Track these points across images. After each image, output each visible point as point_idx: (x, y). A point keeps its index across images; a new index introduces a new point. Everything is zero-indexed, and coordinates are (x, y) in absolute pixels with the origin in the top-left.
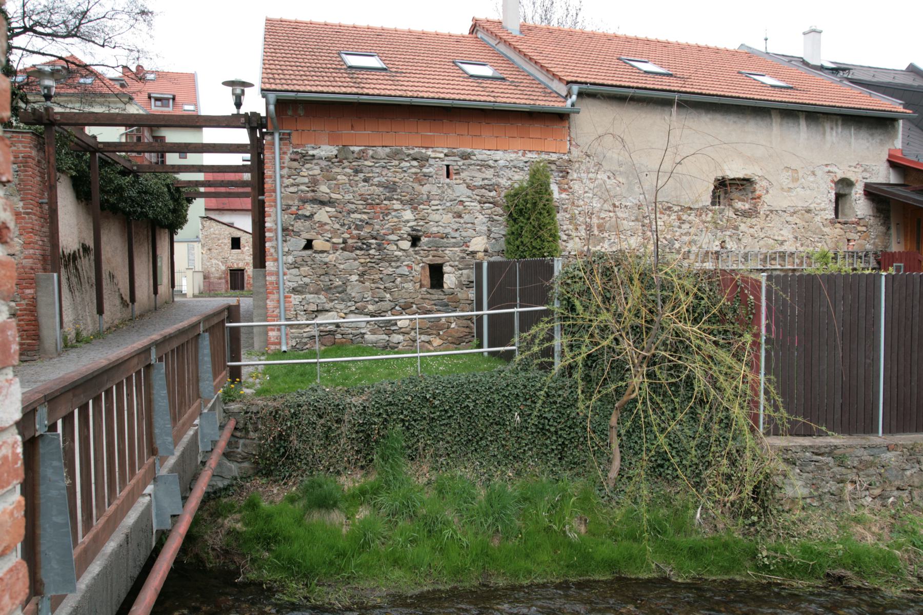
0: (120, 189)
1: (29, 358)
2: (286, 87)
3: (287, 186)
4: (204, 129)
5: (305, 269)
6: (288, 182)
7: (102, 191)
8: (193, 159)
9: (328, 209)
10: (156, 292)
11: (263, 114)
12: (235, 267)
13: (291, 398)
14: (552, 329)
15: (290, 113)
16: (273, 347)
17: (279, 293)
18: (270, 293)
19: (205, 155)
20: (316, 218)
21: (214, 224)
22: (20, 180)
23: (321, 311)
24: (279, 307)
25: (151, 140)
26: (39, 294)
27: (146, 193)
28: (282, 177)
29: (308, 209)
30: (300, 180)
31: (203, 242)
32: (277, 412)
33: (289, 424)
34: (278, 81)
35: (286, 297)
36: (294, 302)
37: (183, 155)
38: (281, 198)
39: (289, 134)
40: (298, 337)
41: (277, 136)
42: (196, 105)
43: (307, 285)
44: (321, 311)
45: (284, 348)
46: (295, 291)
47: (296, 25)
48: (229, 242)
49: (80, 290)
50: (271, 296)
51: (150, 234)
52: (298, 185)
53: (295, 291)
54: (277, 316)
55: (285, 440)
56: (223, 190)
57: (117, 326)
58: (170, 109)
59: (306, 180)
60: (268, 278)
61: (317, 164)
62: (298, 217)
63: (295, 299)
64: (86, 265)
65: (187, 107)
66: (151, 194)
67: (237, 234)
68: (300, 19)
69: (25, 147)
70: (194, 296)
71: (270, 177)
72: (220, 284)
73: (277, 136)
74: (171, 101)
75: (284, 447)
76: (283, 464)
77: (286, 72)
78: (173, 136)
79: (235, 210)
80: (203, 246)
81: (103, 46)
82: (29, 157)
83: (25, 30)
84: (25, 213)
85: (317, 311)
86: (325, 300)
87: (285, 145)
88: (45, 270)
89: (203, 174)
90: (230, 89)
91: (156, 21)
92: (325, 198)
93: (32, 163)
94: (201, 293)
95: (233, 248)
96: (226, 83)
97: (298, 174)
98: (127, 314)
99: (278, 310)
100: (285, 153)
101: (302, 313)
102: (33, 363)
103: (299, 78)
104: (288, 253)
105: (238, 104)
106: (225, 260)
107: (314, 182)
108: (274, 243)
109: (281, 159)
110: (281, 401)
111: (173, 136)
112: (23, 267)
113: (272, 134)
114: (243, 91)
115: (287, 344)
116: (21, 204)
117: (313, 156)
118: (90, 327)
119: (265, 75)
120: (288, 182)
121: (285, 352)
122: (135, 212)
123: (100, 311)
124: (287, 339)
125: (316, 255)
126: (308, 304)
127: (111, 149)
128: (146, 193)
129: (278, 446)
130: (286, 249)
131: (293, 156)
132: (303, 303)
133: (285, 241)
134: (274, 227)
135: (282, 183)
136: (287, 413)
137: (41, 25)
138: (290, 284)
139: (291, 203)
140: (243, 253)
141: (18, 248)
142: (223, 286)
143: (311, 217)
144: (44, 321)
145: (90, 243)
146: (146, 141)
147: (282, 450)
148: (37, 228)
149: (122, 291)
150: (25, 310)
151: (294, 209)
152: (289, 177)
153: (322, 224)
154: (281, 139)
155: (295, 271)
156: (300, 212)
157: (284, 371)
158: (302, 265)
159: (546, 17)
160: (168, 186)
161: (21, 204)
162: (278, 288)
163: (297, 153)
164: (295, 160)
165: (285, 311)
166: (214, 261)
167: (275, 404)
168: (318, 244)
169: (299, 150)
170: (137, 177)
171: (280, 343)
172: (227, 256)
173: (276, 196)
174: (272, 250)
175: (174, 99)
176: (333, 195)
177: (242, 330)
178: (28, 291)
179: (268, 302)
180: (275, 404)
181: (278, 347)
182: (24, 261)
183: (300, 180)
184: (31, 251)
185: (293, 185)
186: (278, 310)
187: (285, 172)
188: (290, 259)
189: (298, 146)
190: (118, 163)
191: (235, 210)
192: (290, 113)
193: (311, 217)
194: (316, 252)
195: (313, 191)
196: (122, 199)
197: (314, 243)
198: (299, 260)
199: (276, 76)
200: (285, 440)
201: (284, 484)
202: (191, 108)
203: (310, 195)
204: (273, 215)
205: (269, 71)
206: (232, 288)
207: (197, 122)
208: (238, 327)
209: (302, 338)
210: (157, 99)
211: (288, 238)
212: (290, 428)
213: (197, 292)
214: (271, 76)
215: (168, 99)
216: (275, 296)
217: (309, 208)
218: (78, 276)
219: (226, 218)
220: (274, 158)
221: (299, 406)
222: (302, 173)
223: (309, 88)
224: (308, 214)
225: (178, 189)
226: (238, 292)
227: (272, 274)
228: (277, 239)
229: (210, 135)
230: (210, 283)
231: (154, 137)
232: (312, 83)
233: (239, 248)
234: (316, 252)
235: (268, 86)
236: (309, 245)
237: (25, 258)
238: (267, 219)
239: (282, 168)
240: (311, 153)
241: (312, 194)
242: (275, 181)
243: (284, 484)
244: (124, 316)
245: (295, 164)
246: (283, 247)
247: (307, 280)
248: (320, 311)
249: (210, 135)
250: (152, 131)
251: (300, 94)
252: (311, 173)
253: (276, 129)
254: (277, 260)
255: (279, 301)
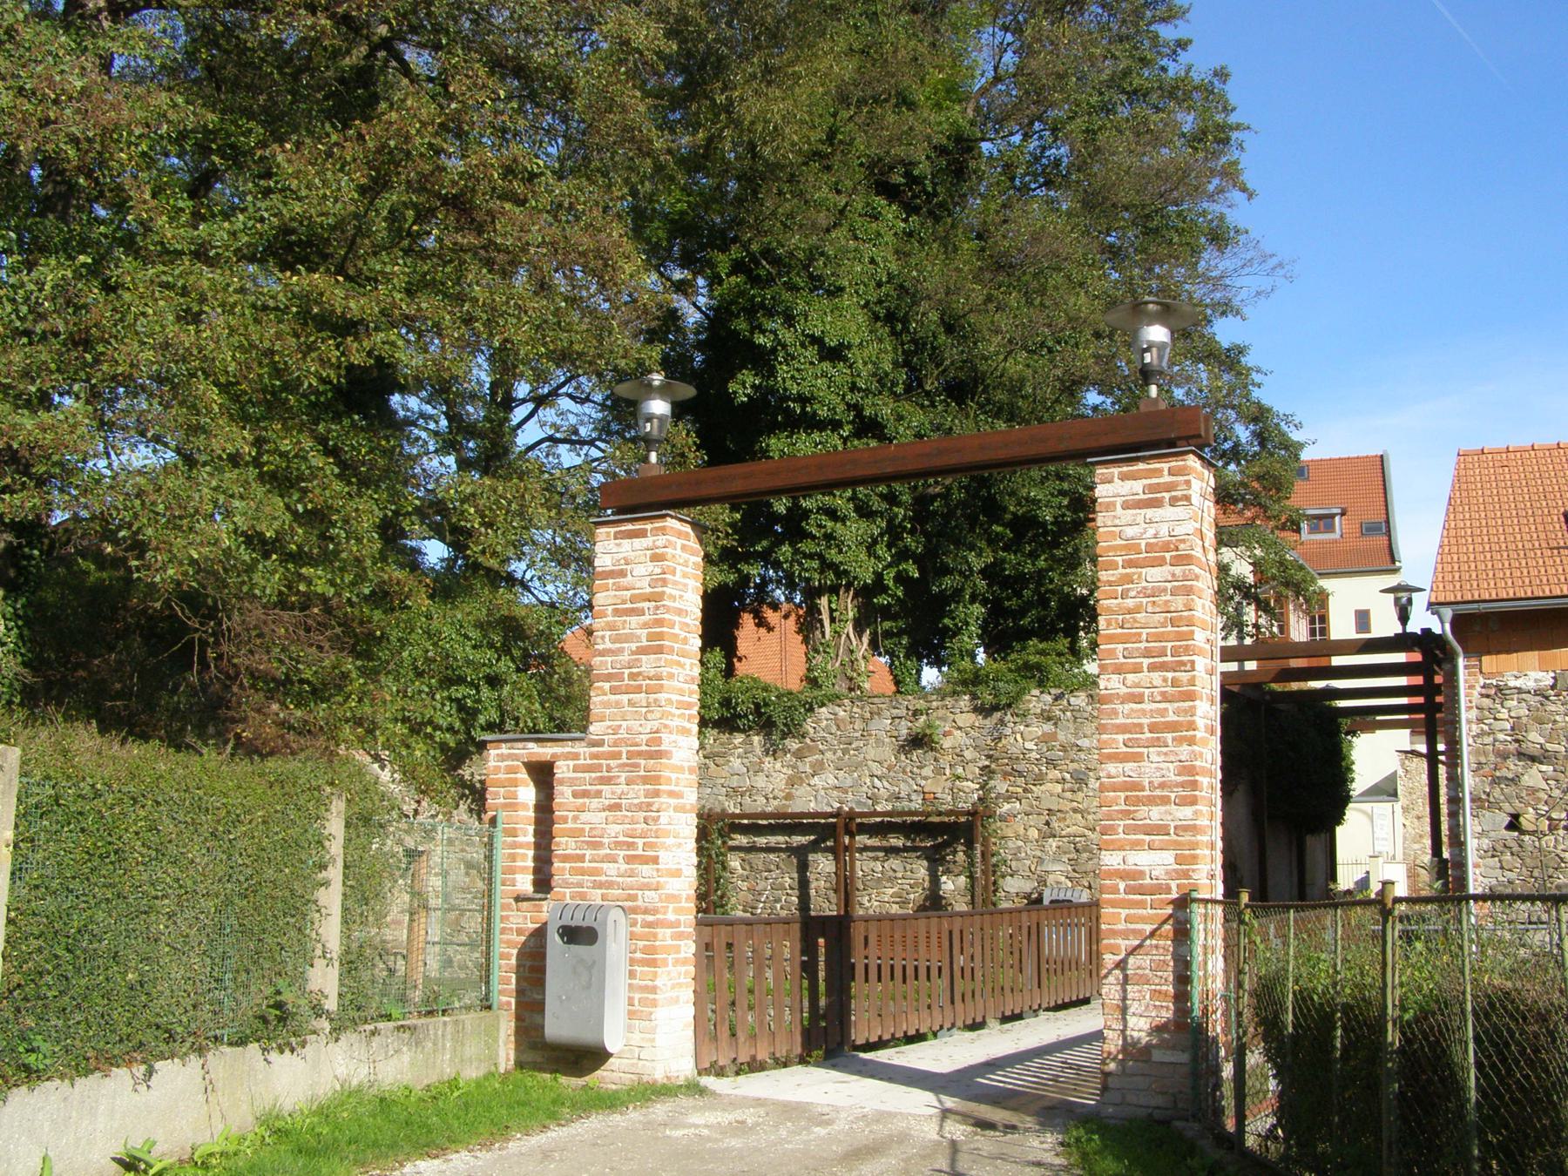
9: (1544, 768)
62: (1496, 781)
92: (1533, 749)
105: (1404, 617)
114: (1410, 601)
146: (732, 387)
153: (1533, 791)
159: (562, 782)
176: (1549, 746)
192: (1477, 628)
224: (1510, 776)
236: (1514, 824)
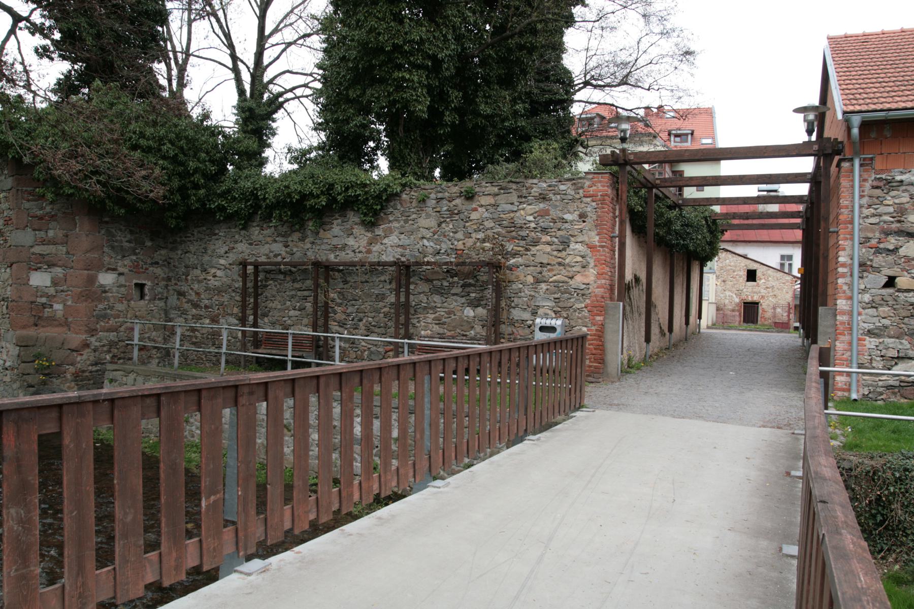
0: (669, 222)
1: (593, 380)
2: (873, 107)
3: (867, 217)
4: (722, 162)
5: (885, 310)
6: (866, 212)
7: (656, 226)
8: (709, 192)
10: (687, 323)
11: (263, 155)
12: (750, 299)
13: (895, 460)
14: (175, 290)
15: (873, 135)
16: (840, 393)
17: (851, 334)
18: (840, 334)
19: (722, 188)
20: (902, 252)
21: (730, 255)
22: (598, 216)
23: (903, 358)
24: (851, 350)
25: (671, 174)
26: (607, 321)
27: (687, 225)
28: (861, 207)
29: (892, 242)
30: (882, 209)
31: (718, 273)
32: (874, 473)
33: (892, 489)
34: (861, 102)
35: (859, 339)
36: (868, 346)
37: (700, 188)
38: (860, 230)
39: (871, 159)
40: (872, 385)
41: (857, 163)
42: (713, 138)
43: (886, 327)
44: (903, 358)
45: (854, 396)
46: (870, 333)
47: (865, 39)
48: (744, 274)
49: (632, 319)
50: (842, 338)
51: (685, 264)
52: (880, 216)
53: (870, 333)
54: (847, 360)
55: (884, 507)
56: (750, 222)
57: (657, 354)
58: (689, 144)
59: (891, 209)
60: (838, 317)
61: (906, 191)
62: (878, 251)
63: (871, 343)
64: (638, 296)
65: (704, 141)
66: (691, 226)
67: (753, 266)
68: (869, 30)
69: (603, 186)
70: (708, 327)
71: (847, 207)
72: (734, 316)
73: (857, 163)
74: (690, 136)
75: (882, 515)
76: (880, 534)
77: (868, 90)
78: (691, 170)
79: (750, 242)
80: (717, 277)
81: (649, 90)
82: (606, 195)
83: (586, 84)
84: (600, 246)
85: (898, 358)
86: (909, 346)
87: (865, 171)
88: (612, 299)
89: (777, 205)
90: (801, 116)
91: (699, 60)
93: (608, 200)
94: (714, 324)
95: (748, 280)
96: (797, 111)
97: (881, 203)
98: (664, 343)
99: (849, 353)
100: (865, 180)
101: (878, 359)
102: (598, 384)
103: (885, 95)
104: (865, 291)
106: (739, 293)
107: (901, 211)
108: (848, 280)
109: (860, 186)
110: (882, 461)
111: (691, 170)
112: (596, 296)
113: (851, 160)
115: (858, 391)
116: (597, 238)
117: (902, 181)
118: (638, 355)
119: (845, 97)
120: (866, 212)
121: (855, 400)
122: (678, 244)
123: (648, 340)
124: (858, 386)
125: (900, 294)
126: (887, 348)
127: (666, 184)
128: (687, 225)
129: (873, 511)
130: (862, 287)
131: (875, 184)
132: (880, 348)
133: (861, 278)
134: (850, 262)
135: (861, 212)
136: (889, 475)
137: (595, 80)
138: (865, 325)
139: (870, 235)
140: (758, 285)
141: (592, 278)
142: (738, 319)
143: (896, 250)
144: (609, 346)
145: (643, 277)
147: (879, 518)
148: (608, 260)
149: (661, 320)
150: (595, 335)
151: (874, 242)
152: (870, 206)
154: (861, 165)
155: (872, 311)
156: (882, 246)
157: (871, 424)
158: (881, 305)
160: (706, 218)
161: (597, 238)
162: (851, 329)
163: (880, 179)
164: (877, 187)
165: (858, 354)
166: (728, 293)
167: (873, 463)
168: (903, 281)
169: (884, 176)
170: (681, 209)
171: (849, 390)
172: (741, 288)
173: (853, 228)
174: (845, 288)
175: (692, 134)
177: (831, 374)
178: (598, 318)
179: (837, 343)
180: (873, 463)
181: (846, 394)
182: (597, 290)
183: (882, 209)
184: (603, 281)
185: (874, 215)
186: (849, 353)
187: (865, 201)
188: (867, 298)
189: (882, 171)
190: (667, 197)
191: (750, 242)
193: (896, 250)
194: (899, 290)
195: (899, 221)
196: (669, 232)
197: (897, 280)
198: (877, 299)
199: (858, 96)
200: (884, 507)
201: (882, 558)
202: (709, 141)
203: (895, 226)
204: (848, 249)
205: (848, 92)
206: (744, 321)
207: (716, 155)
208: (828, 372)
209: (877, 386)
210: (676, 136)
211: (865, 274)
212: (894, 493)
213: (710, 324)
214: (852, 97)
215: (687, 135)
216: (846, 338)
217: (893, 241)
218: (631, 305)
219: (740, 250)
220: (853, 186)
221: (906, 470)
222: (885, 202)
223: (903, 105)
224: (891, 247)
225: (714, 222)
226: (752, 326)
227: (843, 313)
228: (851, 275)
229: (728, 168)
230: (724, 315)
231: (673, 172)
232: (905, 98)
233: (755, 281)
234: (899, 290)
235: (851, 108)
236: (891, 282)
237: (598, 287)
238: (841, 253)
239: (861, 197)
240: (898, 178)
241: (898, 225)
242: (853, 211)
243: (882, 558)
244: (662, 345)
245: (878, 192)
246: (859, 284)
247: (886, 322)
248: (901, 358)
249: (728, 168)
250: (671, 167)
251: (891, 113)
252: (897, 201)
253: (856, 154)
254: (851, 298)
255: (850, 344)
